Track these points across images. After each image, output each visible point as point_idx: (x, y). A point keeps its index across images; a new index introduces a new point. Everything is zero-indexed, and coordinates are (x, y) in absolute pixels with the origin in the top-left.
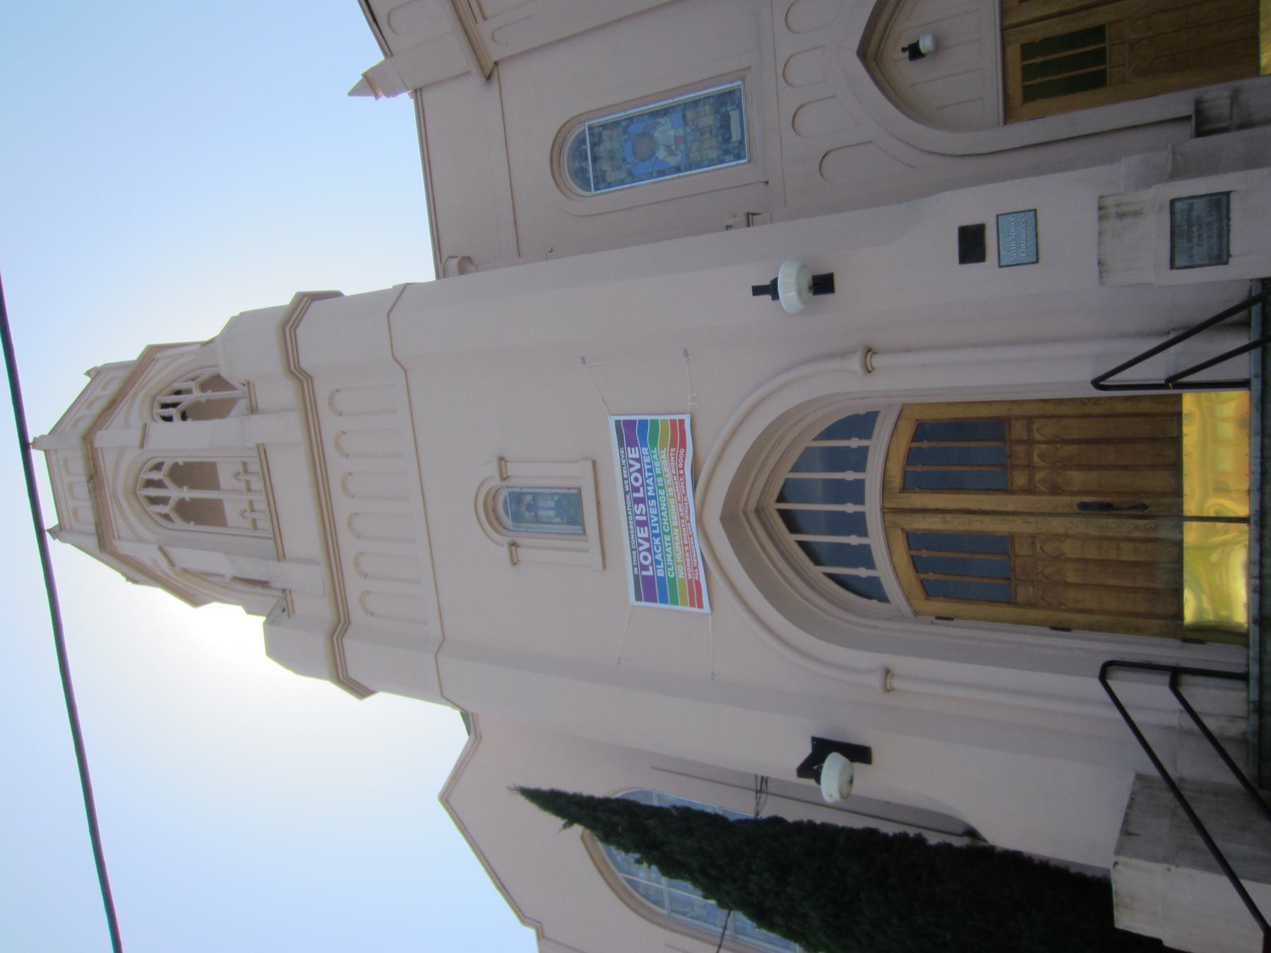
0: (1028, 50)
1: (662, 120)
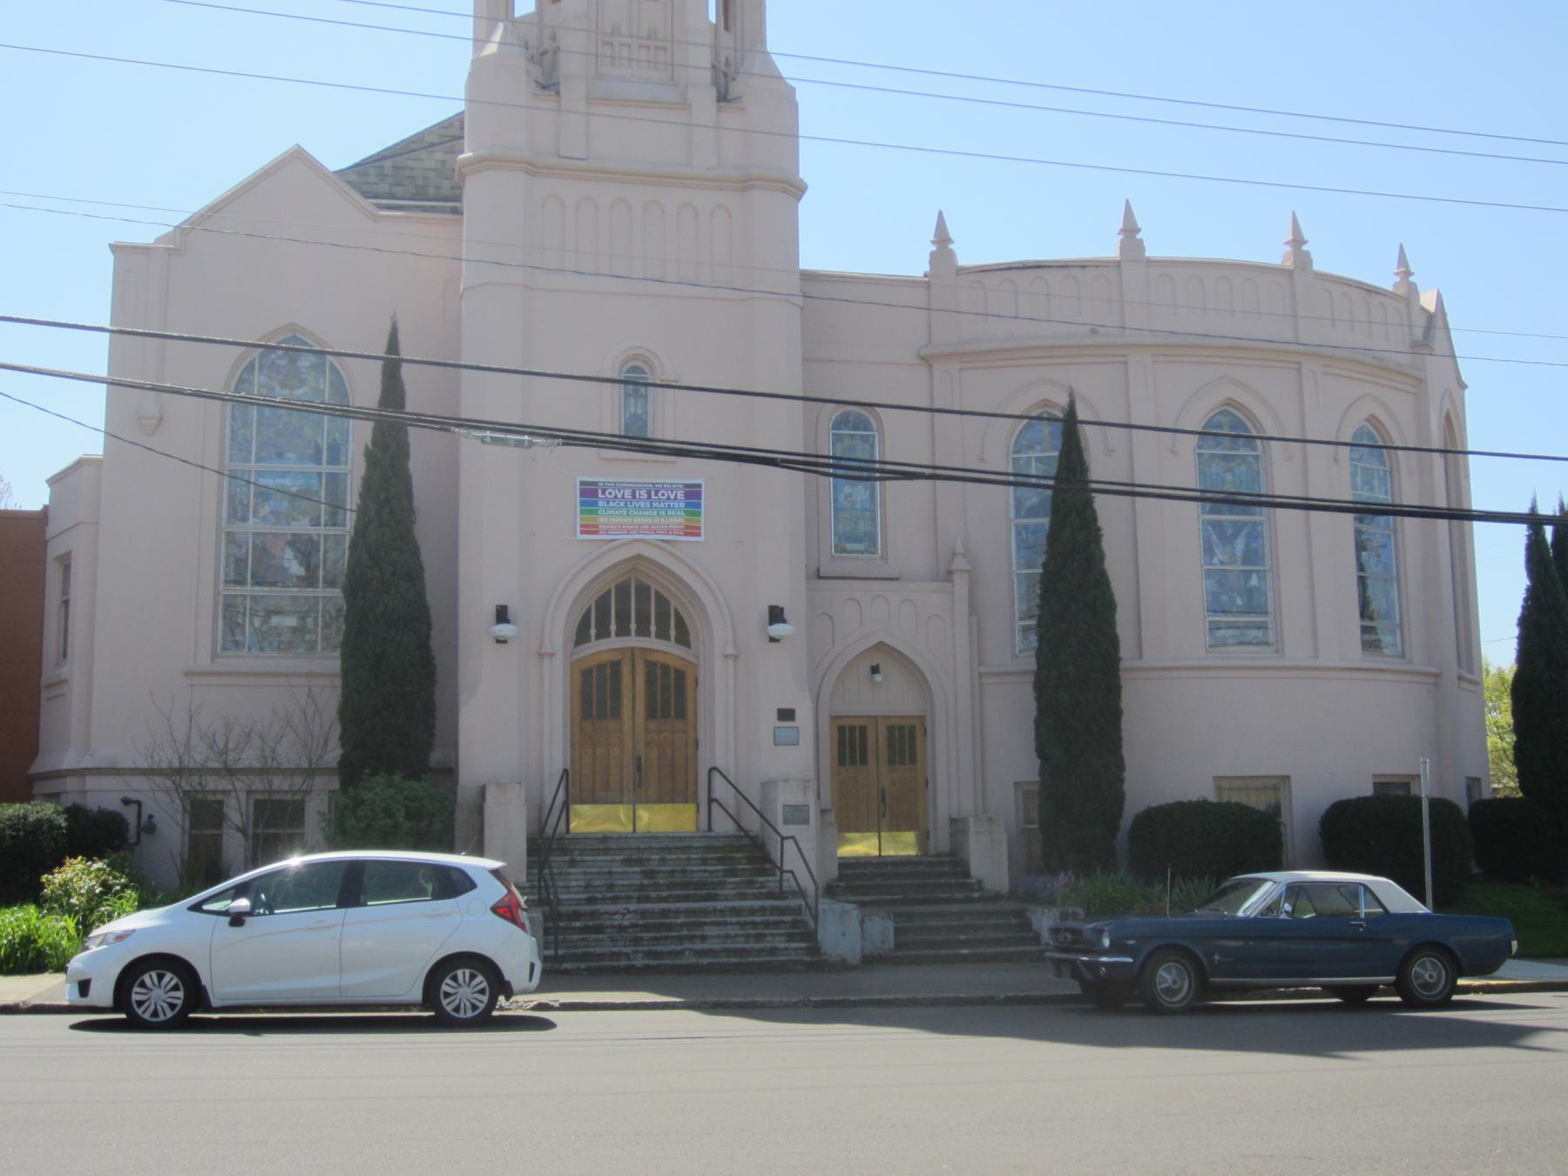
0: (863, 729)
1: (868, 493)
